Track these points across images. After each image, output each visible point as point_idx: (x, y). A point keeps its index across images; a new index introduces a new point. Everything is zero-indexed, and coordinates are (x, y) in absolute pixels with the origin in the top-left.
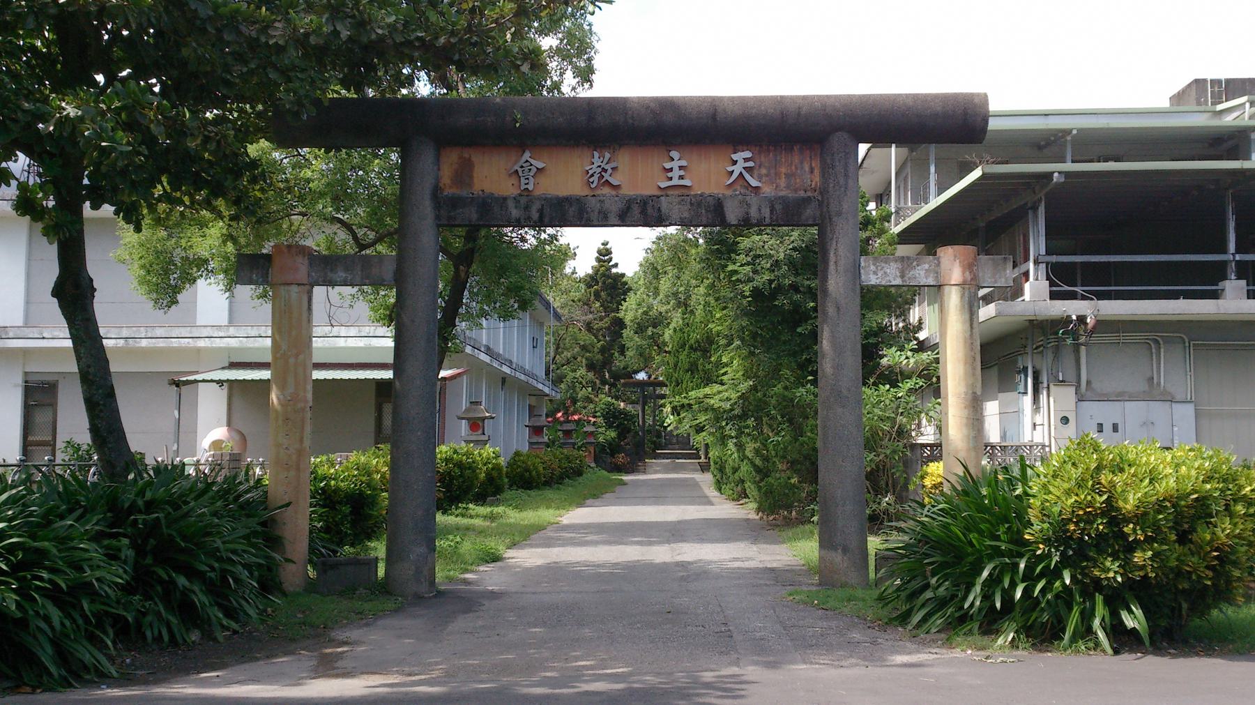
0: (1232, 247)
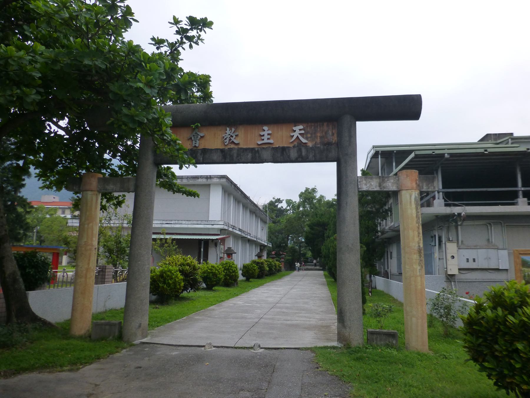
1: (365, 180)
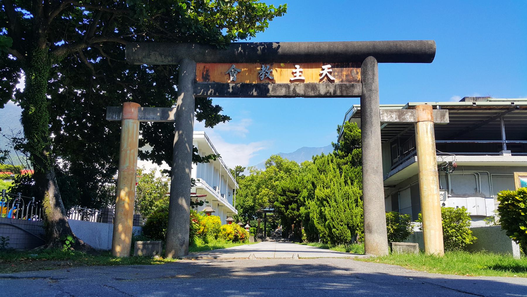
0: (504, 137)
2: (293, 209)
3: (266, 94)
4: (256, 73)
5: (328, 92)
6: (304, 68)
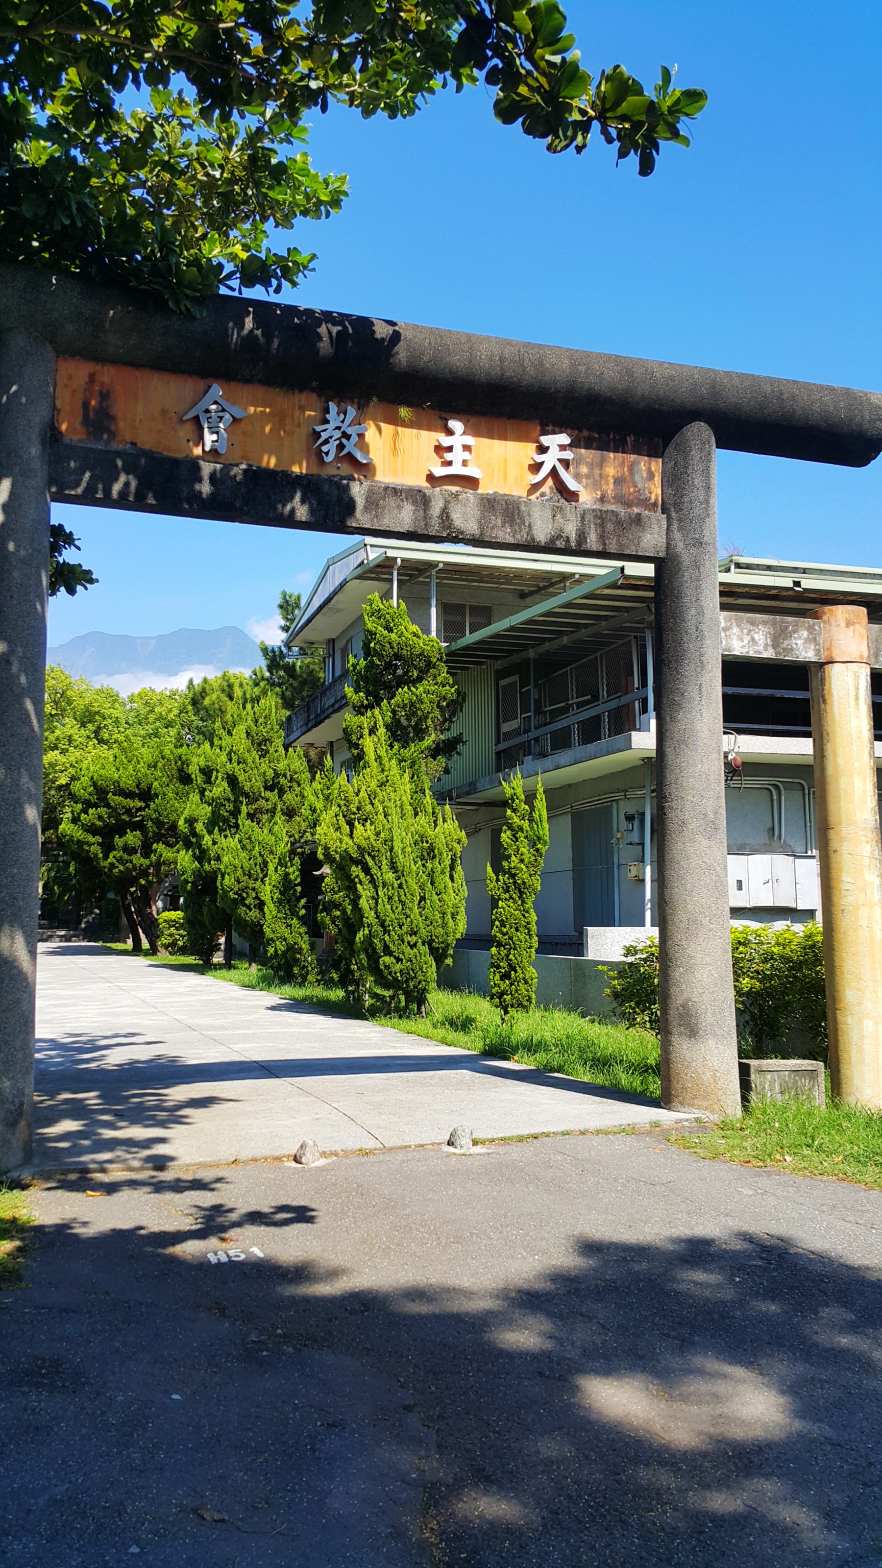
1: (738, 626)
2: (129, 850)
3: (343, 522)
4: (304, 431)
5: (559, 537)
6: (477, 434)
